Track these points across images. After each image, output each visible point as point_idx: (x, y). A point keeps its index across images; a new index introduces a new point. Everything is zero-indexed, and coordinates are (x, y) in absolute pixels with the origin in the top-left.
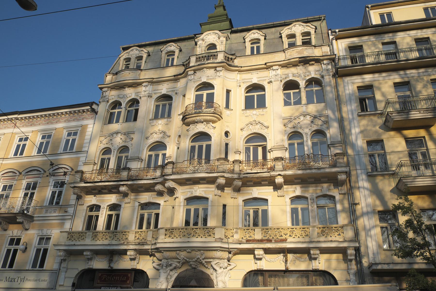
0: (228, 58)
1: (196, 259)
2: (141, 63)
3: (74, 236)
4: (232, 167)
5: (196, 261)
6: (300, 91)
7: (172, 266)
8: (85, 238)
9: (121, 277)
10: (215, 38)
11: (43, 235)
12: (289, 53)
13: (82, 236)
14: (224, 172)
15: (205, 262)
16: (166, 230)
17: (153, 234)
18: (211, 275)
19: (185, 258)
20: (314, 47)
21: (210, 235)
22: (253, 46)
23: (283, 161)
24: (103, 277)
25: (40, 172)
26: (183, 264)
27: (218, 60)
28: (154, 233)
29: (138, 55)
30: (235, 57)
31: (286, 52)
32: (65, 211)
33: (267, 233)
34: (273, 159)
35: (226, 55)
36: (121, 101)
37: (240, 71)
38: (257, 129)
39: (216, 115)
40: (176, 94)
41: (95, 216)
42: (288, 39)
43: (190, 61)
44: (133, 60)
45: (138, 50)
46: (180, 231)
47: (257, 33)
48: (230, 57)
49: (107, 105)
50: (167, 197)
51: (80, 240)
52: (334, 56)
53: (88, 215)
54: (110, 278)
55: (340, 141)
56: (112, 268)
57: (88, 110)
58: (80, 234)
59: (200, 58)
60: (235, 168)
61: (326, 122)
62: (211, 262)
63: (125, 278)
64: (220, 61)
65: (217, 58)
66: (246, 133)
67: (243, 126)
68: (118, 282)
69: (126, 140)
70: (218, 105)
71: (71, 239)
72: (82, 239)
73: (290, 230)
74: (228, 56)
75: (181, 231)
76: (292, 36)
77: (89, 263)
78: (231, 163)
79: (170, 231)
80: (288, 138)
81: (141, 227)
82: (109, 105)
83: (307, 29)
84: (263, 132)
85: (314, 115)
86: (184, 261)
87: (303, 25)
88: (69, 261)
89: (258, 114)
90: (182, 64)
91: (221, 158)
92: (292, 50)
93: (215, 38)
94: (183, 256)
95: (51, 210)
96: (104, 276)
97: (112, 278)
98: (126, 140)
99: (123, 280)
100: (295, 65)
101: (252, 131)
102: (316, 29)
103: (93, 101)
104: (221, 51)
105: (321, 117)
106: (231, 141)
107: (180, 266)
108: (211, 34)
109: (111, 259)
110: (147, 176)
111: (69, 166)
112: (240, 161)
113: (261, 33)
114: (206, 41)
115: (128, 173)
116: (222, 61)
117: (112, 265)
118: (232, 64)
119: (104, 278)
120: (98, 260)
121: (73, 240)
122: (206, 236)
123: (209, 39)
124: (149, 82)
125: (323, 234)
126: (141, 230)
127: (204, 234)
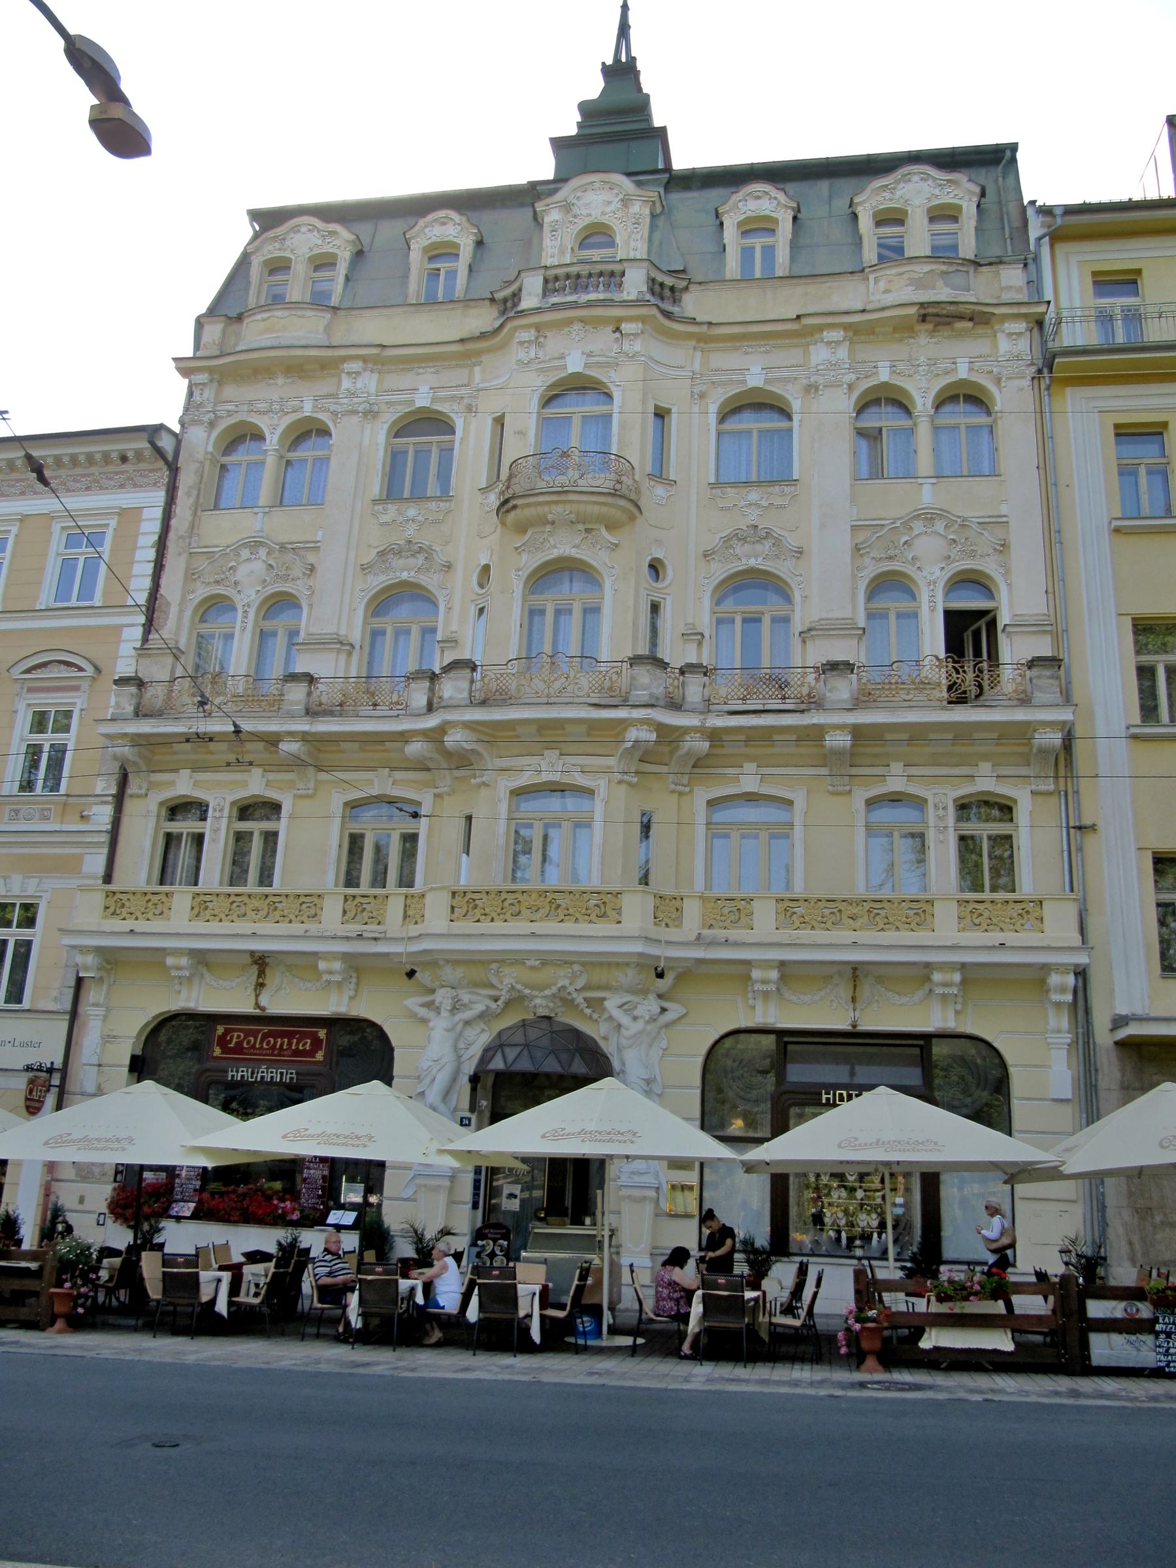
0: (662, 285)
1: (554, 989)
2: (333, 280)
3: (127, 904)
4: (678, 687)
5: (554, 995)
6: (912, 431)
7: (471, 1009)
8: (166, 911)
9: (295, 1040)
10: (610, 203)
11: (9, 894)
12: (882, 285)
13: (156, 904)
14: (652, 706)
15: (585, 999)
16: (454, 894)
17: (406, 906)
18: (602, 1044)
19: (518, 987)
20: (971, 269)
21: (604, 915)
22: (748, 241)
23: (854, 677)
24: (232, 1037)
25: (81, 669)
26: (508, 1004)
27: (625, 292)
28: (409, 901)
29: (316, 251)
30: (684, 283)
31: (871, 277)
32: (82, 817)
33: (878, 914)
34: (818, 668)
35: (654, 274)
36: (263, 423)
37: (701, 339)
38: (752, 558)
39: (622, 503)
40: (469, 409)
41: (188, 834)
42: (932, 219)
43: (520, 290)
44: (300, 269)
45: (319, 231)
46: (502, 898)
47: (767, 193)
48: (669, 281)
49: (209, 436)
50: (445, 779)
51: (150, 915)
52: (1042, 309)
53: (163, 830)
54: (255, 1043)
55: (1045, 615)
56: (263, 1009)
57: (139, 454)
58: (149, 896)
59: (556, 279)
60: (686, 693)
61: (1002, 545)
62: (604, 999)
63: (306, 1043)
64: (633, 297)
65: (621, 285)
66: (720, 570)
67: (714, 541)
68: (284, 1056)
69: (289, 572)
70: (627, 464)
71: (118, 912)
72: (157, 912)
73: (867, 906)
74: (660, 278)
75: (505, 899)
76: (891, 218)
77: (184, 994)
78: (673, 673)
79: (466, 899)
80: (716, 598)
81: (351, 880)
82: (216, 440)
83: (947, 197)
84: (782, 568)
85: (959, 517)
86: (515, 994)
87: (934, 179)
88: (112, 983)
89: (764, 503)
90: (490, 296)
91: (1039, 659)
92: (894, 271)
93: (610, 203)
94: (512, 981)
95: (31, 811)
96: (236, 1034)
97: (261, 1043)
98: (289, 572)
99: (301, 1048)
100: (901, 329)
101: (744, 561)
102: (983, 194)
103: (158, 422)
104: (632, 256)
105: (985, 526)
106: (669, 594)
107: (499, 1011)
108: (597, 185)
109: (261, 980)
110: (378, 708)
111: (87, 659)
112: (705, 670)
113: (781, 197)
114: (576, 211)
115: (309, 694)
116: (640, 297)
117: (264, 1000)
118: (675, 309)
119: (235, 1040)
120: (213, 983)
121: (124, 915)
122: (593, 917)
123: (587, 204)
124: (364, 359)
125: (977, 921)
126: (266, 890)
127: (499, 910)
